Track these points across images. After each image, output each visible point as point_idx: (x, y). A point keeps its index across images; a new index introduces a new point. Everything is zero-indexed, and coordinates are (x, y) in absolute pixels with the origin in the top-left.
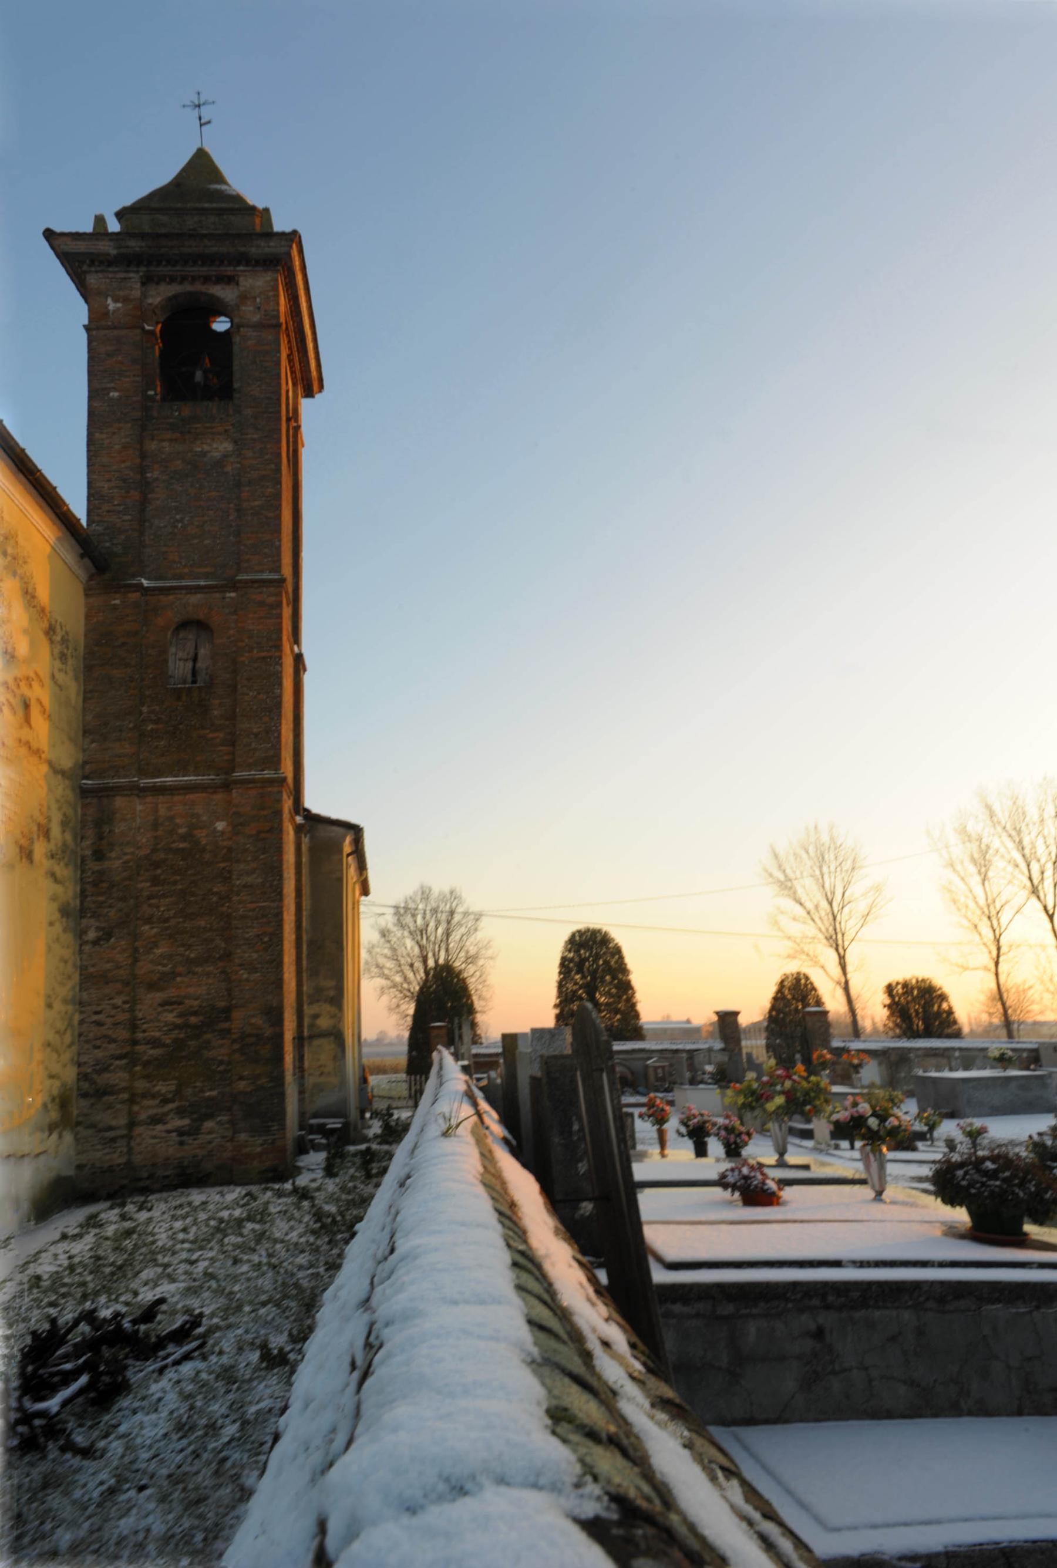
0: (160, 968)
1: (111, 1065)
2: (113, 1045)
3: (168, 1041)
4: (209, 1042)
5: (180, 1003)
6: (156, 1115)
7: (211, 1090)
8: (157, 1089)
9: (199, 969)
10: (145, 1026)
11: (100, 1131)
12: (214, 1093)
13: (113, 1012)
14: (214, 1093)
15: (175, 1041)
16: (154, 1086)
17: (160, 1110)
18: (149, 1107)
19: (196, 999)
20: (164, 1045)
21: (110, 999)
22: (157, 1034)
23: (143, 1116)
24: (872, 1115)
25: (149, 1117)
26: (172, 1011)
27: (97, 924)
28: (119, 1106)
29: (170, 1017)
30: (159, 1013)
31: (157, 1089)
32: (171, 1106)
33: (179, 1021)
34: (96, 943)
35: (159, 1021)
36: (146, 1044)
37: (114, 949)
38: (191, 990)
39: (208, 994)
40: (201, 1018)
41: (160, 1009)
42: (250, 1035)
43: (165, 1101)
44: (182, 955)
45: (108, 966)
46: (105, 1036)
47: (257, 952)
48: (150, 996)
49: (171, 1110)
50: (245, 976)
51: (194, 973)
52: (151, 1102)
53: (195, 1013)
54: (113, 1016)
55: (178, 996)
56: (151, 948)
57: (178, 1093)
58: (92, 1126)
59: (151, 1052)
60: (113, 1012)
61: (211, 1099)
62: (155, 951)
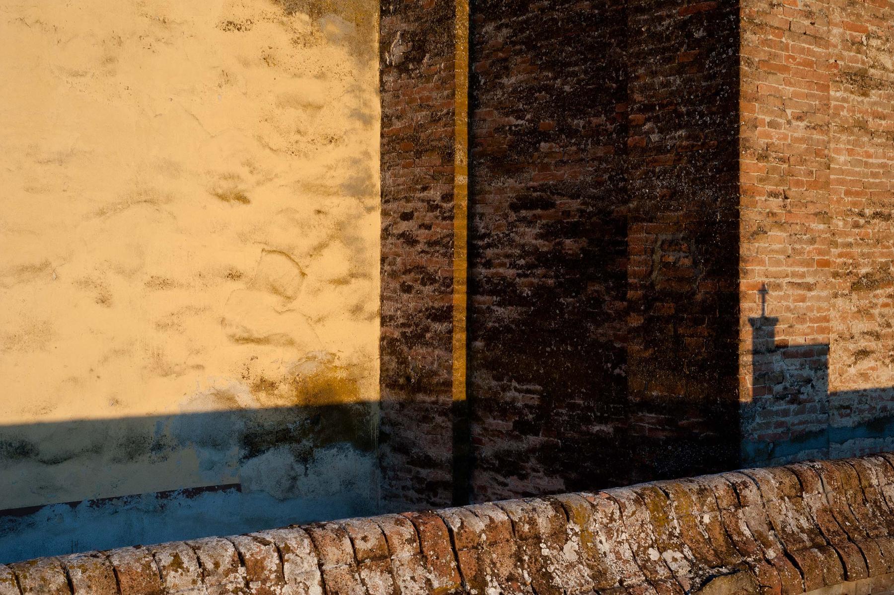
0: (512, 119)
1: (427, 329)
2: (428, 289)
3: (527, 292)
4: (598, 301)
5: (547, 205)
6: (509, 453)
7: (601, 420)
8: (509, 395)
9: (578, 123)
10: (490, 252)
11: (413, 462)
12: (608, 428)
13: (429, 217)
14: (608, 428)
15: (540, 290)
16: (505, 389)
17: (514, 445)
18: (499, 433)
19: (572, 197)
20: (521, 301)
21: (424, 189)
22: (510, 273)
23: (487, 451)
24: (661, 553)
25: (497, 456)
26: (530, 223)
27: (404, 26)
28: (439, 419)
29: (529, 236)
30: (512, 225)
31: (509, 395)
32: (533, 440)
33: (544, 246)
34: (402, 68)
35: (511, 242)
36: (491, 293)
37: (428, 79)
38: (565, 173)
39: (598, 184)
40: (584, 242)
41: (513, 216)
42: (665, 295)
43: (523, 428)
44: (548, 89)
45: (421, 116)
46: (420, 269)
47: (679, 72)
48: (498, 184)
49: (532, 450)
50: (655, 137)
51: (572, 133)
52: (504, 425)
53: (573, 231)
54: (428, 227)
55: (542, 188)
56: (498, 76)
57: (543, 411)
58: (402, 448)
59: (500, 311)
60: (429, 217)
61: (599, 438)
62: (505, 80)
